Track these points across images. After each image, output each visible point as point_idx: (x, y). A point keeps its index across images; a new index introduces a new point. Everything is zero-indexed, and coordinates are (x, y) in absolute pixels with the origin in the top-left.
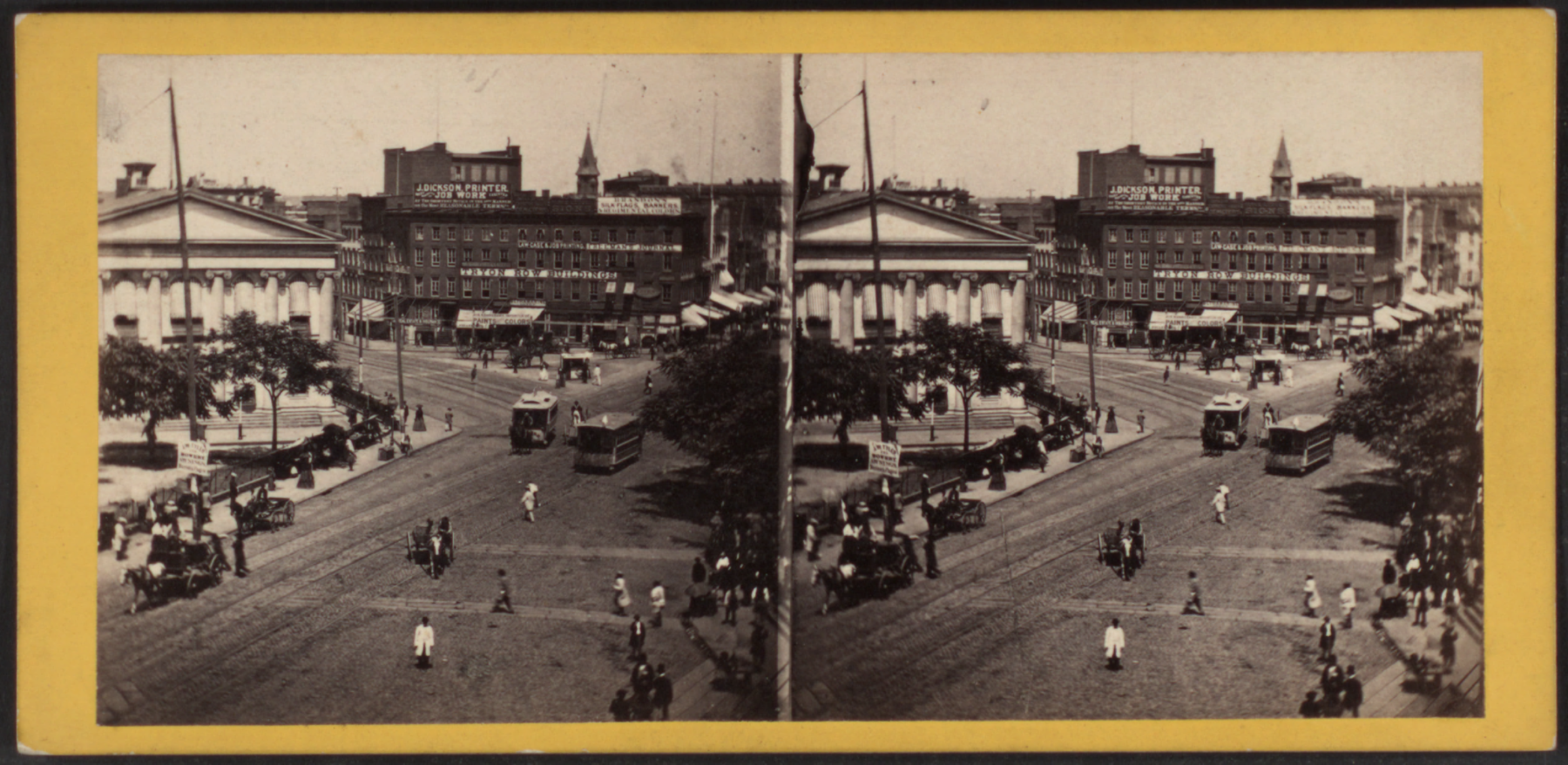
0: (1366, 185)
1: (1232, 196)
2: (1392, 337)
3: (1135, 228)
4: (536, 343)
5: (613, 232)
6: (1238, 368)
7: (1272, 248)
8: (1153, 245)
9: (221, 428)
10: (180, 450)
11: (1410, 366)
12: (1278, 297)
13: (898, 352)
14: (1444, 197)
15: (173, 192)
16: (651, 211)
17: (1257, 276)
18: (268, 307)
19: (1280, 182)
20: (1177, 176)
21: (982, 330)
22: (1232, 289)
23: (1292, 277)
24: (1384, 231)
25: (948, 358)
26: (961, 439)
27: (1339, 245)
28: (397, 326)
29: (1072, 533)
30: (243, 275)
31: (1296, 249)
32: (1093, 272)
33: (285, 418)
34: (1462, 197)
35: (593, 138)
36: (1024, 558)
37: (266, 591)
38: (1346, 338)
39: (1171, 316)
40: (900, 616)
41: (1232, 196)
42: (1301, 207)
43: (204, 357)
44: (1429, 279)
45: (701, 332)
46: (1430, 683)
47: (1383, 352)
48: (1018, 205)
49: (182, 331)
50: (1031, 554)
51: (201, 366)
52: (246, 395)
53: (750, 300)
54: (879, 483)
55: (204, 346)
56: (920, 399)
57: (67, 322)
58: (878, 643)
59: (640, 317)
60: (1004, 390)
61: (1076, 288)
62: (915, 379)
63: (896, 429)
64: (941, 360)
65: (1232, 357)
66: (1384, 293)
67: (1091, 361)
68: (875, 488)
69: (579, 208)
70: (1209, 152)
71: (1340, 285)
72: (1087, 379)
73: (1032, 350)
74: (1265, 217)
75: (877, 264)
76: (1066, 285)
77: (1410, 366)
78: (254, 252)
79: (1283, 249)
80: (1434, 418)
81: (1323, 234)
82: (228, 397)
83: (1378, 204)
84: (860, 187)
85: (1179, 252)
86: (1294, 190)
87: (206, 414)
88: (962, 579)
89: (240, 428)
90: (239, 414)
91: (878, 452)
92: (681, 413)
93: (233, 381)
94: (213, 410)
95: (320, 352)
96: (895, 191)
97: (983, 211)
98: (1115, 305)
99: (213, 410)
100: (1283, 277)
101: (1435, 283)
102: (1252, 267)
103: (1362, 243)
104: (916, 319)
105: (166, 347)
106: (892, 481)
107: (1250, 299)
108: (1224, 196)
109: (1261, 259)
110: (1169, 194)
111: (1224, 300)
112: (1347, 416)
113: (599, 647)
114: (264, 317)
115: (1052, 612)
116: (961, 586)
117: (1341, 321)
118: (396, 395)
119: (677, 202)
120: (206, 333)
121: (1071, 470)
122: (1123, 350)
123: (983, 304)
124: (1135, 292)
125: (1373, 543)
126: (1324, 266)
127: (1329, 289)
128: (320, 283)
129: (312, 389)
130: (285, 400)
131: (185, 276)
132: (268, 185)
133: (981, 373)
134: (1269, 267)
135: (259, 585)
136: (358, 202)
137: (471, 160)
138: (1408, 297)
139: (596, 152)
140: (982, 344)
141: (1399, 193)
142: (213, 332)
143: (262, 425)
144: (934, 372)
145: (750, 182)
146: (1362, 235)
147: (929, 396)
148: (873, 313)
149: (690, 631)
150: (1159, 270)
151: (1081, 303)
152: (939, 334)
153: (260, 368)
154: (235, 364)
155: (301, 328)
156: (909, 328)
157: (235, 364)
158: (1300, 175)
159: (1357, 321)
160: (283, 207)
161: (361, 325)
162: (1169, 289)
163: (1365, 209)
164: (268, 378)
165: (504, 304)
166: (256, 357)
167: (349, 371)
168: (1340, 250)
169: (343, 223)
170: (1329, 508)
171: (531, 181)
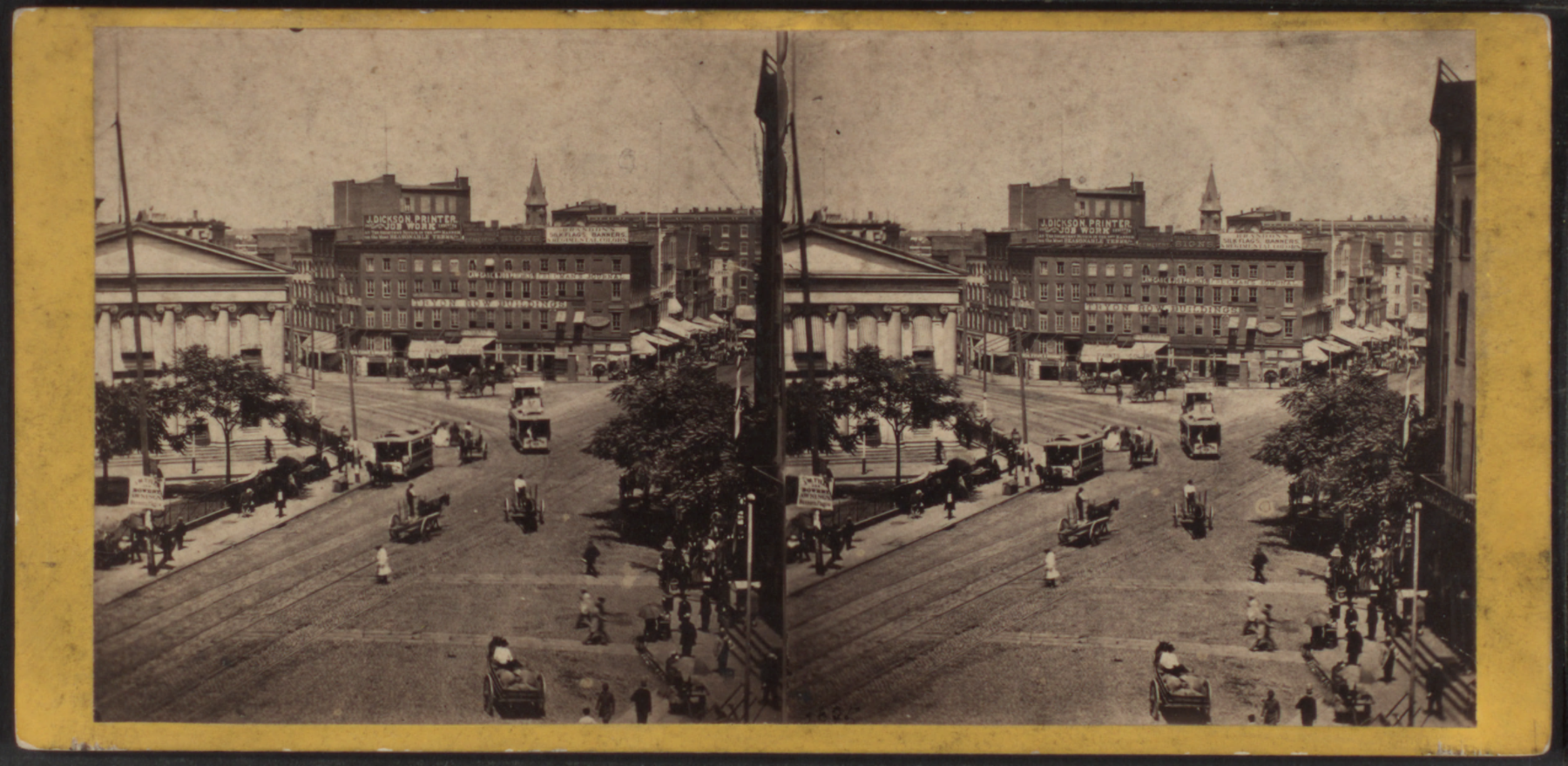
0: (620, 211)
1: (488, 224)
2: (1321, 369)
3: (392, 256)
4: (1161, 378)
5: (562, 261)
7: (528, 276)
8: (1085, 278)
9: (845, 462)
10: (133, 485)
12: (536, 325)
13: (829, 385)
14: (697, 223)
16: (600, 240)
17: (514, 304)
18: (220, 339)
20: (433, 205)
21: (913, 364)
22: (491, 317)
23: (1222, 311)
24: (638, 257)
25: (879, 392)
26: (223, 472)
27: (594, 272)
28: (350, 360)
29: (336, 563)
30: (193, 308)
31: (553, 277)
32: (351, 301)
33: (909, 453)
34: (714, 223)
37: (890, 626)
38: (605, 364)
39: (430, 344)
41: (488, 224)
42: (1230, 239)
43: (155, 391)
44: (1356, 312)
45: (651, 360)
46: (694, 705)
47: (1312, 385)
48: (948, 237)
49: (133, 366)
50: (296, 585)
51: (152, 400)
52: (200, 429)
53: (698, 327)
54: (811, 516)
55: (155, 380)
56: (852, 431)
57: (66, 357)
59: (590, 345)
60: (935, 423)
62: (846, 412)
63: (158, 462)
64: (202, 392)
65: (1163, 389)
66: (1312, 328)
67: (352, 392)
68: (139, 521)
69: (1201, 244)
70: (465, 180)
71: (1270, 318)
73: (292, 382)
74: (1197, 250)
75: (807, 297)
76: (998, 315)
78: (210, 286)
79: (540, 277)
80: (1362, 449)
81: (580, 261)
82: (181, 431)
84: (116, 219)
85: (437, 282)
86: (1224, 224)
87: (158, 449)
88: (894, 612)
89: (194, 462)
90: (192, 448)
91: (809, 486)
92: (1302, 447)
93: (857, 416)
94: (165, 444)
95: (941, 387)
97: (914, 243)
98: (373, 333)
99: (165, 444)
100: (540, 305)
101: (691, 309)
102: (509, 295)
103: (617, 269)
104: (847, 351)
105: (118, 382)
106: (824, 515)
107: (509, 326)
108: (480, 224)
109: (518, 286)
110: (429, 222)
111: (483, 328)
113: (555, 674)
114: (887, 350)
115: (985, 645)
116: (894, 619)
117: (1271, 353)
118: (350, 427)
119: (1298, 237)
120: (158, 366)
121: (333, 501)
122: (383, 379)
125: (1309, 573)
126: (580, 293)
127: (586, 316)
128: (271, 315)
129: (265, 422)
130: (238, 434)
131: (136, 310)
132: (218, 218)
133: (913, 407)
134: (526, 295)
135: (882, 620)
136: (308, 235)
137: (419, 192)
138: (1338, 330)
139: (544, 181)
140: (242, 375)
141: (653, 218)
142: (164, 365)
143: (886, 460)
144: (193, 406)
145: (695, 211)
146: (1290, 268)
147: (861, 429)
148: (803, 347)
149: (1312, 663)
150: (417, 299)
151: (1012, 335)
152: (199, 366)
153: (212, 402)
154: (187, 399)
155: (252, 361)
156: (840, 361)
157: (187, 399)
158: (555, 202)
159: (615, 347)
160: (233, 240)
162: (428, 317)
163: (1293, 242)
164: (220, 412)
165: (1127, 339)
166: (208, 390)
167: (973, 406)
168: (596, 277)
169: (294, 255)
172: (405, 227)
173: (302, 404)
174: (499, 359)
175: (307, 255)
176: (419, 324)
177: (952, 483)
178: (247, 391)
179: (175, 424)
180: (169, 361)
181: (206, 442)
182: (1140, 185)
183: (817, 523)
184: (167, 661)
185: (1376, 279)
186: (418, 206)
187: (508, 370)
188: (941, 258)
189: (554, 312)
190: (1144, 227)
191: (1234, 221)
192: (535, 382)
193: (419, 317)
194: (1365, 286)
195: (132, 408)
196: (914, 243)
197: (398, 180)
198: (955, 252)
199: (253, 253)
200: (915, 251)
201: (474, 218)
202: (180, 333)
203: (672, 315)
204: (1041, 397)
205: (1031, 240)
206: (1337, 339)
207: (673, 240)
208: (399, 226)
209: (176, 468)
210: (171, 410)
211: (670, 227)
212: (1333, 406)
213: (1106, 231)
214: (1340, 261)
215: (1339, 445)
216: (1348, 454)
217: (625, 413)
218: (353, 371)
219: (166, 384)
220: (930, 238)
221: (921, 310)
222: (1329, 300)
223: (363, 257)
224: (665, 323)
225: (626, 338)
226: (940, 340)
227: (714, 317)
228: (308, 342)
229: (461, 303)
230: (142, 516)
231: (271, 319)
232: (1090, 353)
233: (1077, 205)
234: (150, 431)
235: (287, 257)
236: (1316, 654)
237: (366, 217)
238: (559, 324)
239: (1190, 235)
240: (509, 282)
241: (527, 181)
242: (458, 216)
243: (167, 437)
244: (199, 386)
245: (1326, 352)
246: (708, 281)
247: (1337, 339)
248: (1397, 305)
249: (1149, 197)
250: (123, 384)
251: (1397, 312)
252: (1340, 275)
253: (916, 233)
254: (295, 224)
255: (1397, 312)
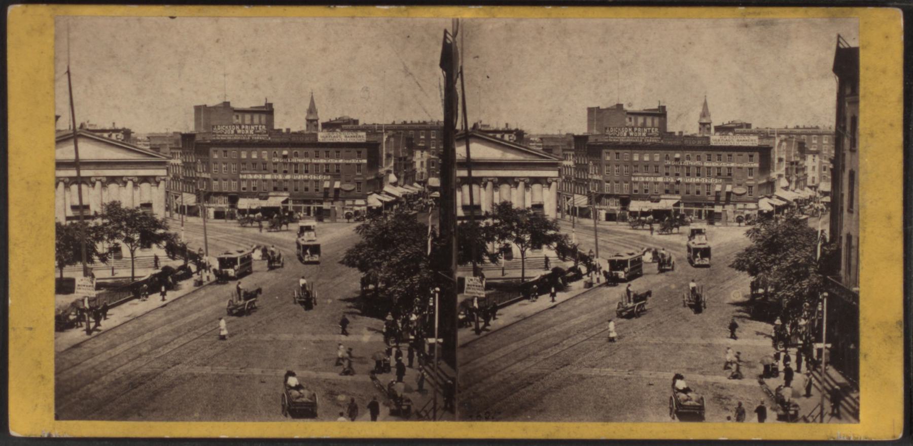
0: (361, 123)
1: (284, 131)
2: (769, 215)
4: (676, 220)
5: (327, 152)
6: (681, 234)
7: (308, 161)
9: (492, 269)
10: (77, 282)
11: (780, 232)
13: (483, 224)
14: (406, 130)
15: (71, 132)
16: (349, 140)
17: (300, 177)
18: (128, 198)
19: (703, 125)
20: (252, 119)
21: (532, 212)
22: (286, 185)
23: (712, 181)
24: (372, 150)
25: (512, 228)
26: (130, 275)
27: (346, 158)
28: (204, 209)
29: (196, 328)
30: (113, 179)
31: (322, 161)
32: (204, 175)
33: (529, 264)
35: (315, 98)
36: (167, 344)
37: (518, 364)
39: (250, 201)
40: (96, 378)
41: (284, 131)
42: (716, 139)
43: (90, 228)
44: (790, 182)
45: (379, 210)
46: (792, 415)
48: (552, 138)
51: (89, 233)
52: (116, 250)
53: (406, 190)
54: (472, 300)
56: (496, 251)
57: (38, 208)
58: (472, 395)
59: (344, 201)
60: (545, 246)
61: (587, 186)
62: (493, 240)
63: (482, 269)
64: (118, 229)
65: (677, 227)
66: (764, 191)
67: (205, 228)
68: (81, 303)
69: (699, 142)
70: (270, 105)
71: (739, 185)
72: (202, 238)
74: (697, 145)
75: (470, 173)
76: (581, 183)
77: (780, 232)
79: (314, 161)
80: (793, 261)
82: (106, 251)
83: (760, 138)
85: (254, 164)
86: (713, 130)
87: (92, 261)
89: (113, 269)
90: (112, 261)
91: (471, 283)
92: (758, 260)
93: (499, 242)
94: (96, 258)
96: (480, 130)
98: (217, 194)
99: (96, 258)
100: (315, 177)
101: (402, 180)
102: (296, 172)
104: (493, 204)
105: (69, 222)
106: (479, 300)
108: (279, 131)
109: (301, 167)
110: (250, 129)
111: (281, 191)
112: (354, 257)
114: (516, 204)
115: (573, 376)
117: (349, 202)
119: (756, 138)
120: (92, 213)
122: (223, 221)
123: (141, 195)
124: (625, 191)
125: (762, 334)
126: (338, 171)
128: (158, 183)
129: (154, 246)
130: (138, 252)
131: (79, 181)
132: (127, 127)
133: (531, 237)
136: (179, 137)
137: (244, 112)
138: (779, 192)
139: (317, 105)
140: (141, 218)
141: (380, 127)
142: (96, 212)
143: (516, 268)
144: (112, 236)
145: (405, 123)
146: (751, 156)
147: (501, 250)
148: (468, 202)
149: (764, 386)
150: (243, 174)
151: (589, 195)
152: (116, 213)
154: (109, 232)
155: (147, 210)
156: (489, 210)
157: (109, 232)
158: (323, 118)
159: (358, 202)
160: (136, 140)
161: (183, 208)
162: (249, 184)
163: (753, 141)
164: (128, 240)
165: (656, 197)
166: (121, 227)
167: (566, 236)
168: (347, 162)
169: (171, 149)
170: (349, 310)
171: (673, 126)
172: (236, 132)
173: (176, 235)
174: (291, 209)
175: (179, 149)
176: (244, 189)
177: (554, 281)
178: (144, 228)
179: (102, 247)
180: (99, 210)
181: (120, 257)
182: (664, 107)
183: (476, 305)
184: (97, 385)
185: (409, 158)
186: (243, 120)
187: (296, 216)
188: (548, 150)
189: (323, 182)
190: (666, 132)
191: (719, 129)
192: (312, 223)
193: (244, 185)
194: (794, 166)
195: (77, 238)
196: (532, 142)
197: (232, 105)
198: (556, 147)
199: (148, 148)
200: (533, 146)
201: (276, 127)
202: (105, 194)
203: (391, 184)
204: (606, 231)
205: (600, 140)
206: (779, 198)
207: (392, 140)
208: (233, 132)
209: (102, 273)
210: (99, 239)
211: (390, 132)
212: (776, 236)
213: (644, 134)
214: (780, 152)
215: (780, 259)
216: (785, 264)
217: (364, 240)
218: (205, 216)
219: (97, 224)
220: (541, 139)
221: (536, 180)
222: (774, 175)
223: (212, 150)
224: (387, 188)
225: (364, 197)
226: (547, 198)
227: (416, 184)
228: (179, 199)
229: (268, 177)
230: (83, 301)
231: (158, 186)
232: (635, 206)
233: (627, 120)
234: (87, 251)
235: (167, 150)
236: (766, 381)
237: (213, 127)
238: (326, 189)
239: (693, 137)
240: (296, 164)
241: (307, 105)
242: (267, 126)
243: (97, 254)
244: (116, 225)
245: (772, 205)
246: (412, 164)
247: (779, 198)
248: (814, 178)
249: (669, 115)
250: (72, 224)
251: (813, 182)
252: (780, 160)
253: (533, 136)
254: (172, 130)
255: (813, 182)
